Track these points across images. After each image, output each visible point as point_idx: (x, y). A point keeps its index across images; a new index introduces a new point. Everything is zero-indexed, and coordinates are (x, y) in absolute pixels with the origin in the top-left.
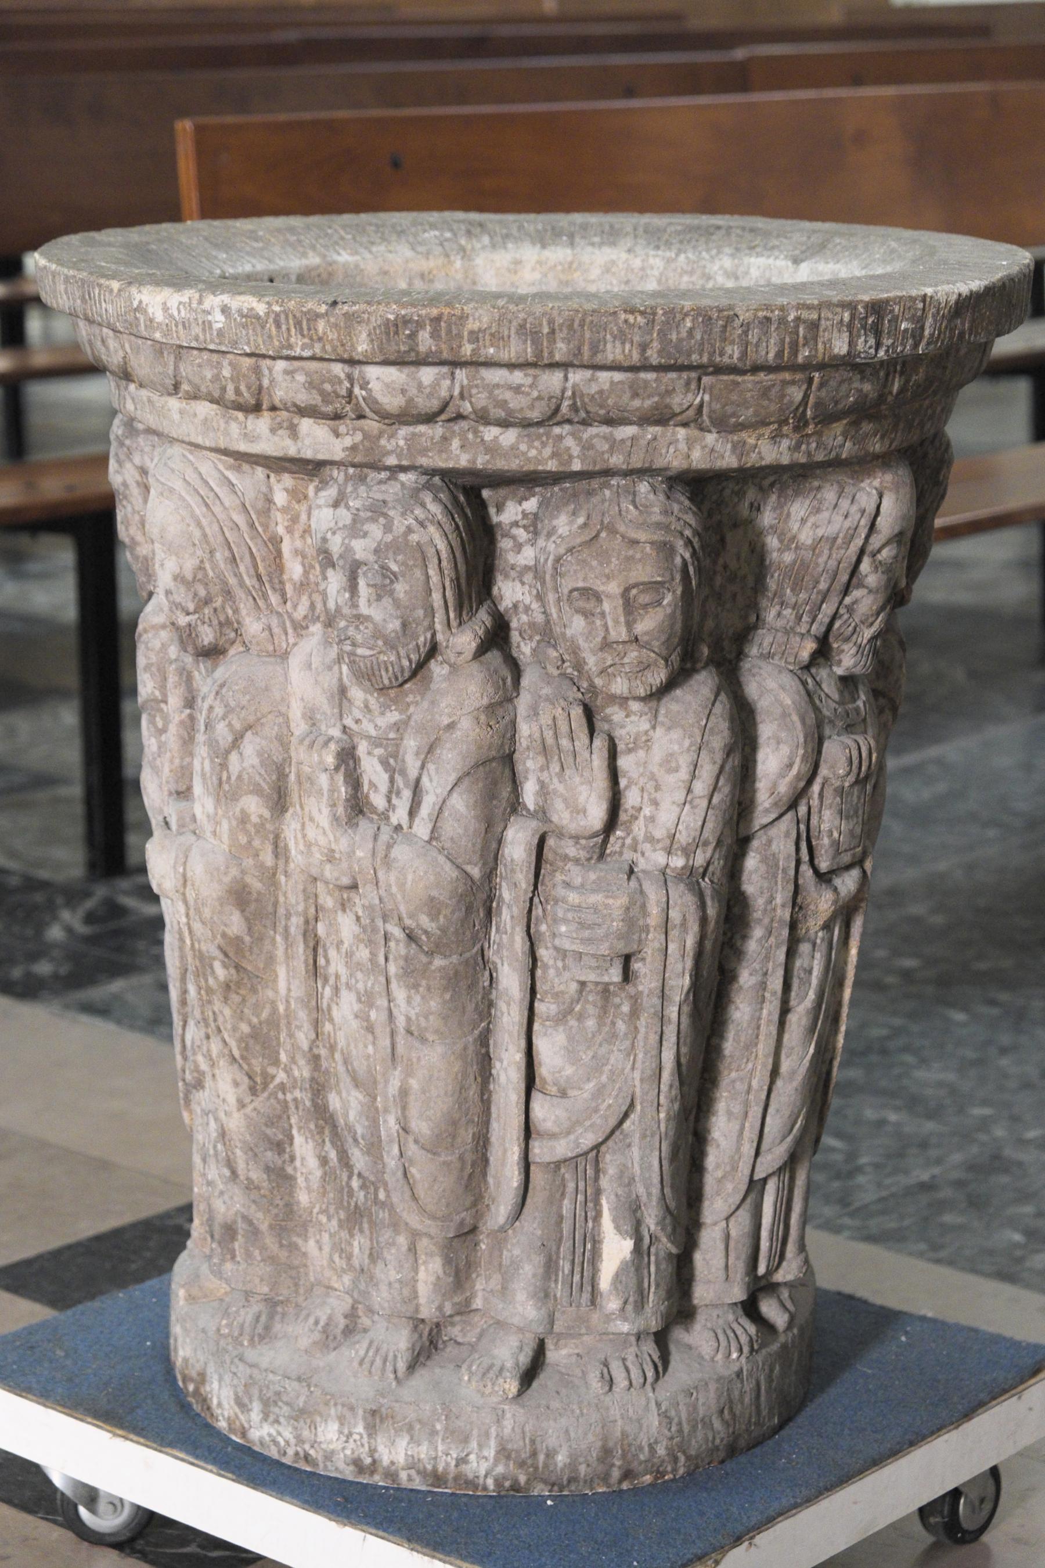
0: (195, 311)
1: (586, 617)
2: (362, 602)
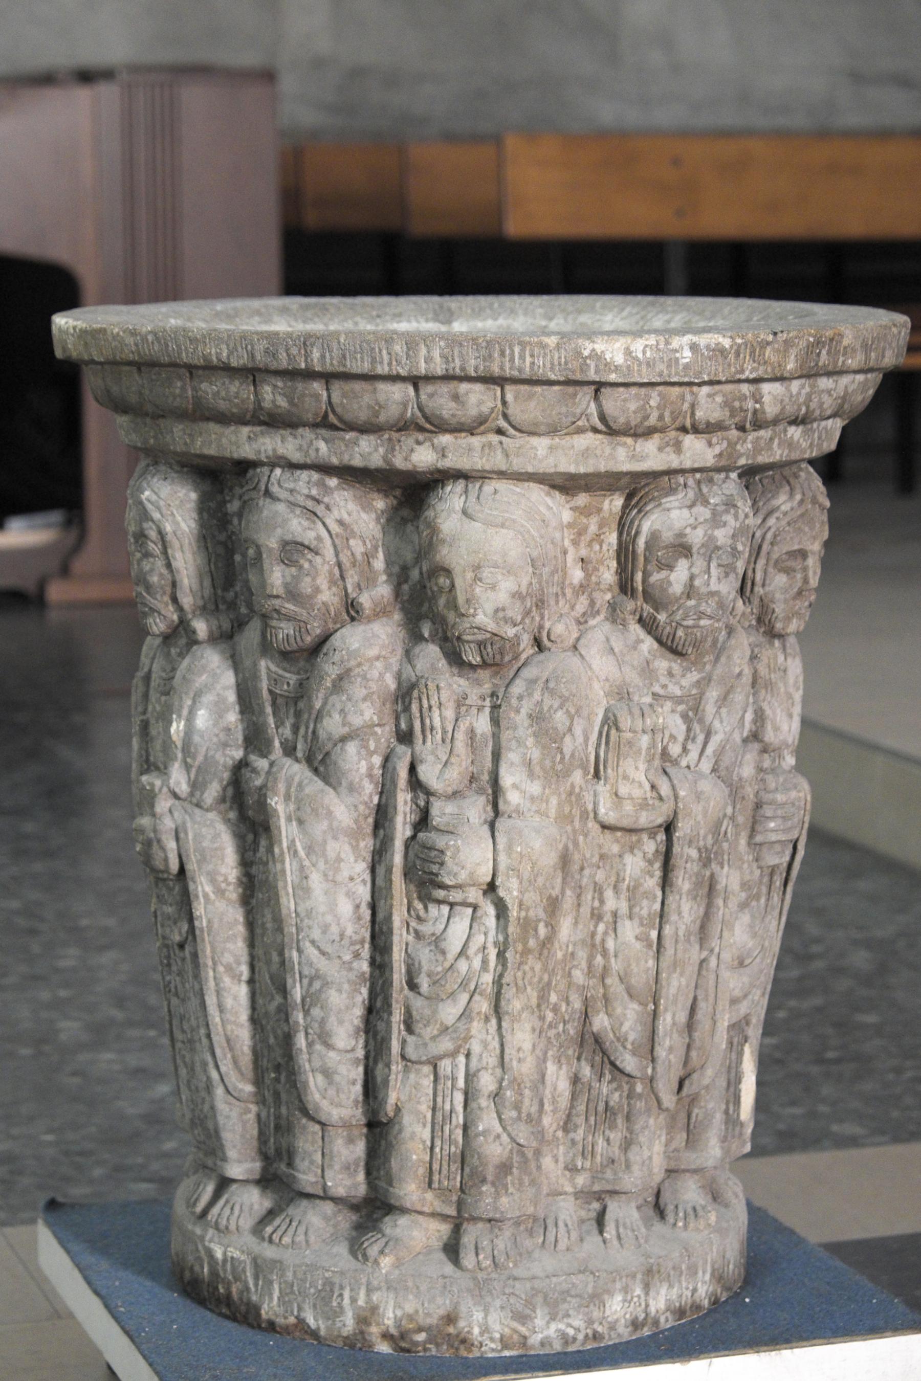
0: (664, 352)
1: (788, 574)
2: (714, 580)
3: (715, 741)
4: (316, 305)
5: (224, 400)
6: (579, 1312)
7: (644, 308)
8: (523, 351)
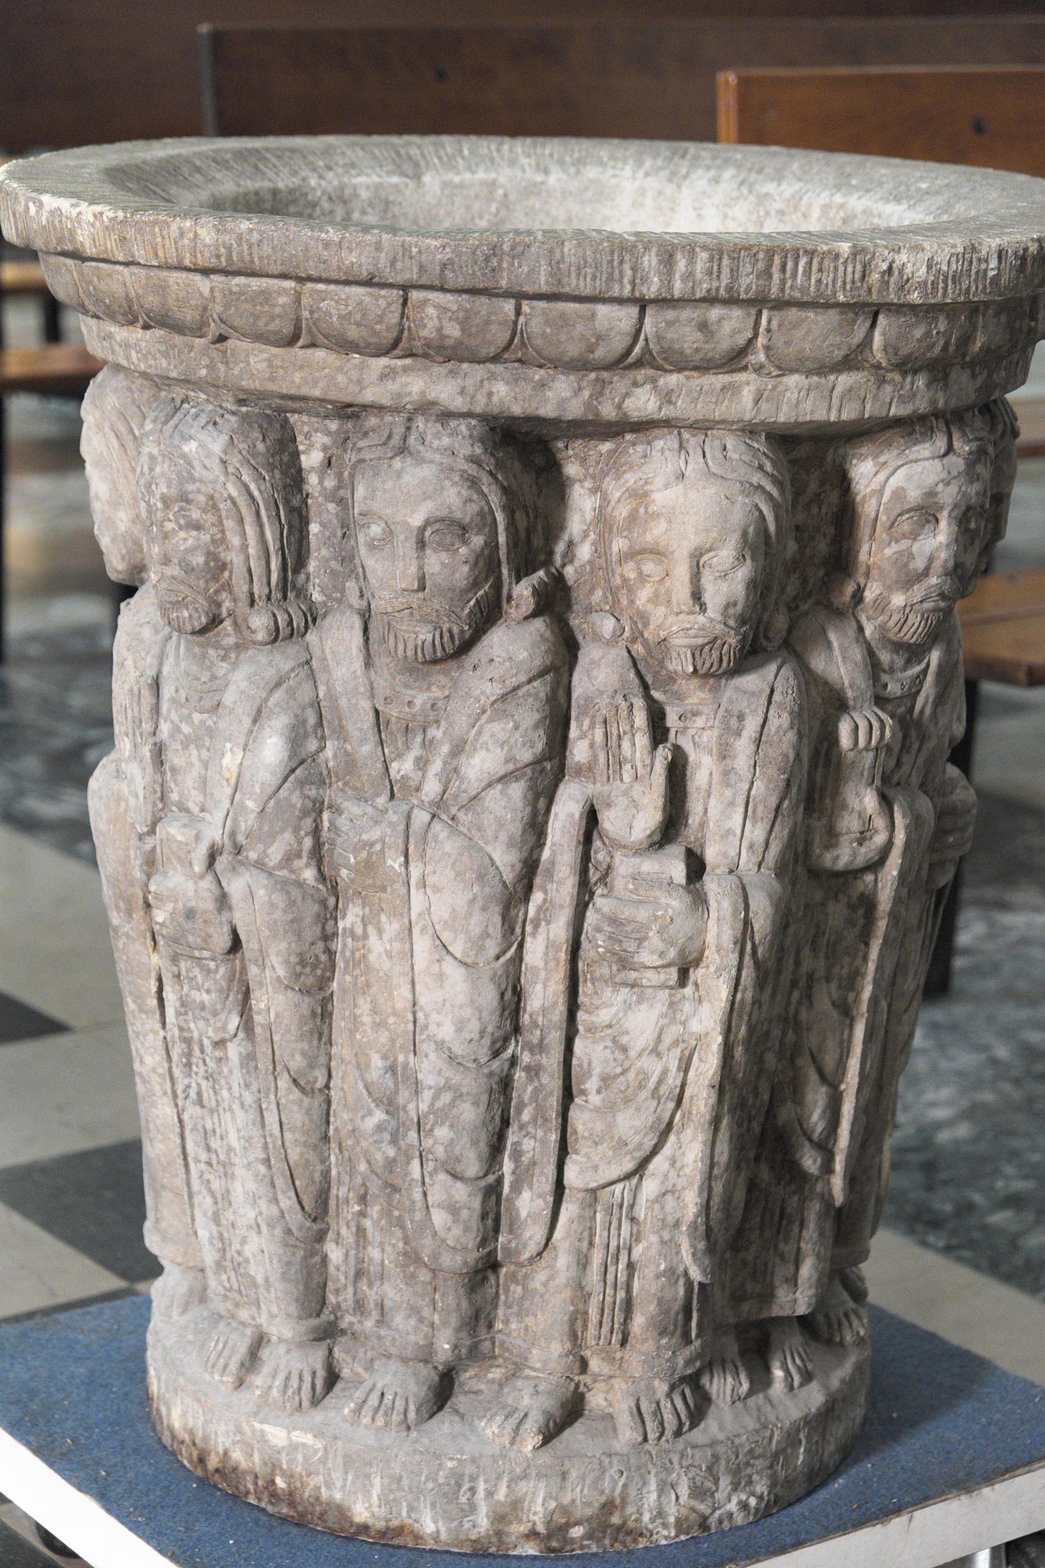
3: (930, 745)
4: (241, 155)
5: (358, 324)
6: (761, 1476)
7: (670, 159)
8: (810, 263)
